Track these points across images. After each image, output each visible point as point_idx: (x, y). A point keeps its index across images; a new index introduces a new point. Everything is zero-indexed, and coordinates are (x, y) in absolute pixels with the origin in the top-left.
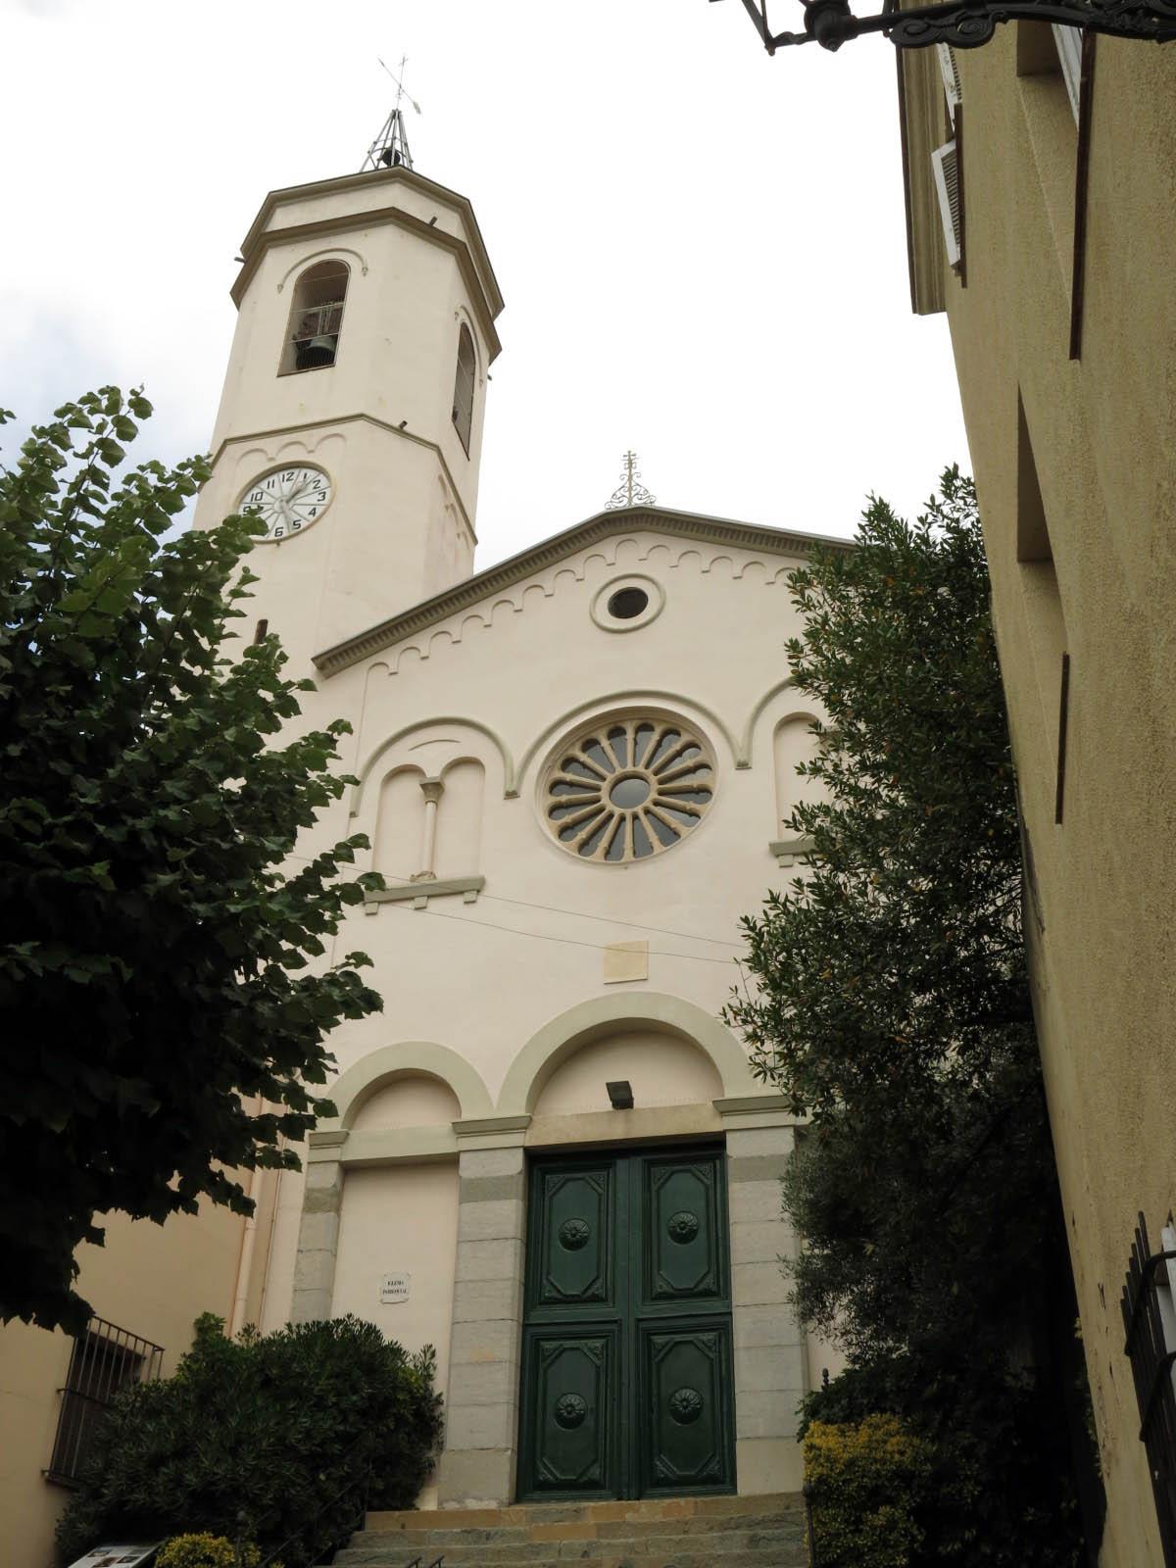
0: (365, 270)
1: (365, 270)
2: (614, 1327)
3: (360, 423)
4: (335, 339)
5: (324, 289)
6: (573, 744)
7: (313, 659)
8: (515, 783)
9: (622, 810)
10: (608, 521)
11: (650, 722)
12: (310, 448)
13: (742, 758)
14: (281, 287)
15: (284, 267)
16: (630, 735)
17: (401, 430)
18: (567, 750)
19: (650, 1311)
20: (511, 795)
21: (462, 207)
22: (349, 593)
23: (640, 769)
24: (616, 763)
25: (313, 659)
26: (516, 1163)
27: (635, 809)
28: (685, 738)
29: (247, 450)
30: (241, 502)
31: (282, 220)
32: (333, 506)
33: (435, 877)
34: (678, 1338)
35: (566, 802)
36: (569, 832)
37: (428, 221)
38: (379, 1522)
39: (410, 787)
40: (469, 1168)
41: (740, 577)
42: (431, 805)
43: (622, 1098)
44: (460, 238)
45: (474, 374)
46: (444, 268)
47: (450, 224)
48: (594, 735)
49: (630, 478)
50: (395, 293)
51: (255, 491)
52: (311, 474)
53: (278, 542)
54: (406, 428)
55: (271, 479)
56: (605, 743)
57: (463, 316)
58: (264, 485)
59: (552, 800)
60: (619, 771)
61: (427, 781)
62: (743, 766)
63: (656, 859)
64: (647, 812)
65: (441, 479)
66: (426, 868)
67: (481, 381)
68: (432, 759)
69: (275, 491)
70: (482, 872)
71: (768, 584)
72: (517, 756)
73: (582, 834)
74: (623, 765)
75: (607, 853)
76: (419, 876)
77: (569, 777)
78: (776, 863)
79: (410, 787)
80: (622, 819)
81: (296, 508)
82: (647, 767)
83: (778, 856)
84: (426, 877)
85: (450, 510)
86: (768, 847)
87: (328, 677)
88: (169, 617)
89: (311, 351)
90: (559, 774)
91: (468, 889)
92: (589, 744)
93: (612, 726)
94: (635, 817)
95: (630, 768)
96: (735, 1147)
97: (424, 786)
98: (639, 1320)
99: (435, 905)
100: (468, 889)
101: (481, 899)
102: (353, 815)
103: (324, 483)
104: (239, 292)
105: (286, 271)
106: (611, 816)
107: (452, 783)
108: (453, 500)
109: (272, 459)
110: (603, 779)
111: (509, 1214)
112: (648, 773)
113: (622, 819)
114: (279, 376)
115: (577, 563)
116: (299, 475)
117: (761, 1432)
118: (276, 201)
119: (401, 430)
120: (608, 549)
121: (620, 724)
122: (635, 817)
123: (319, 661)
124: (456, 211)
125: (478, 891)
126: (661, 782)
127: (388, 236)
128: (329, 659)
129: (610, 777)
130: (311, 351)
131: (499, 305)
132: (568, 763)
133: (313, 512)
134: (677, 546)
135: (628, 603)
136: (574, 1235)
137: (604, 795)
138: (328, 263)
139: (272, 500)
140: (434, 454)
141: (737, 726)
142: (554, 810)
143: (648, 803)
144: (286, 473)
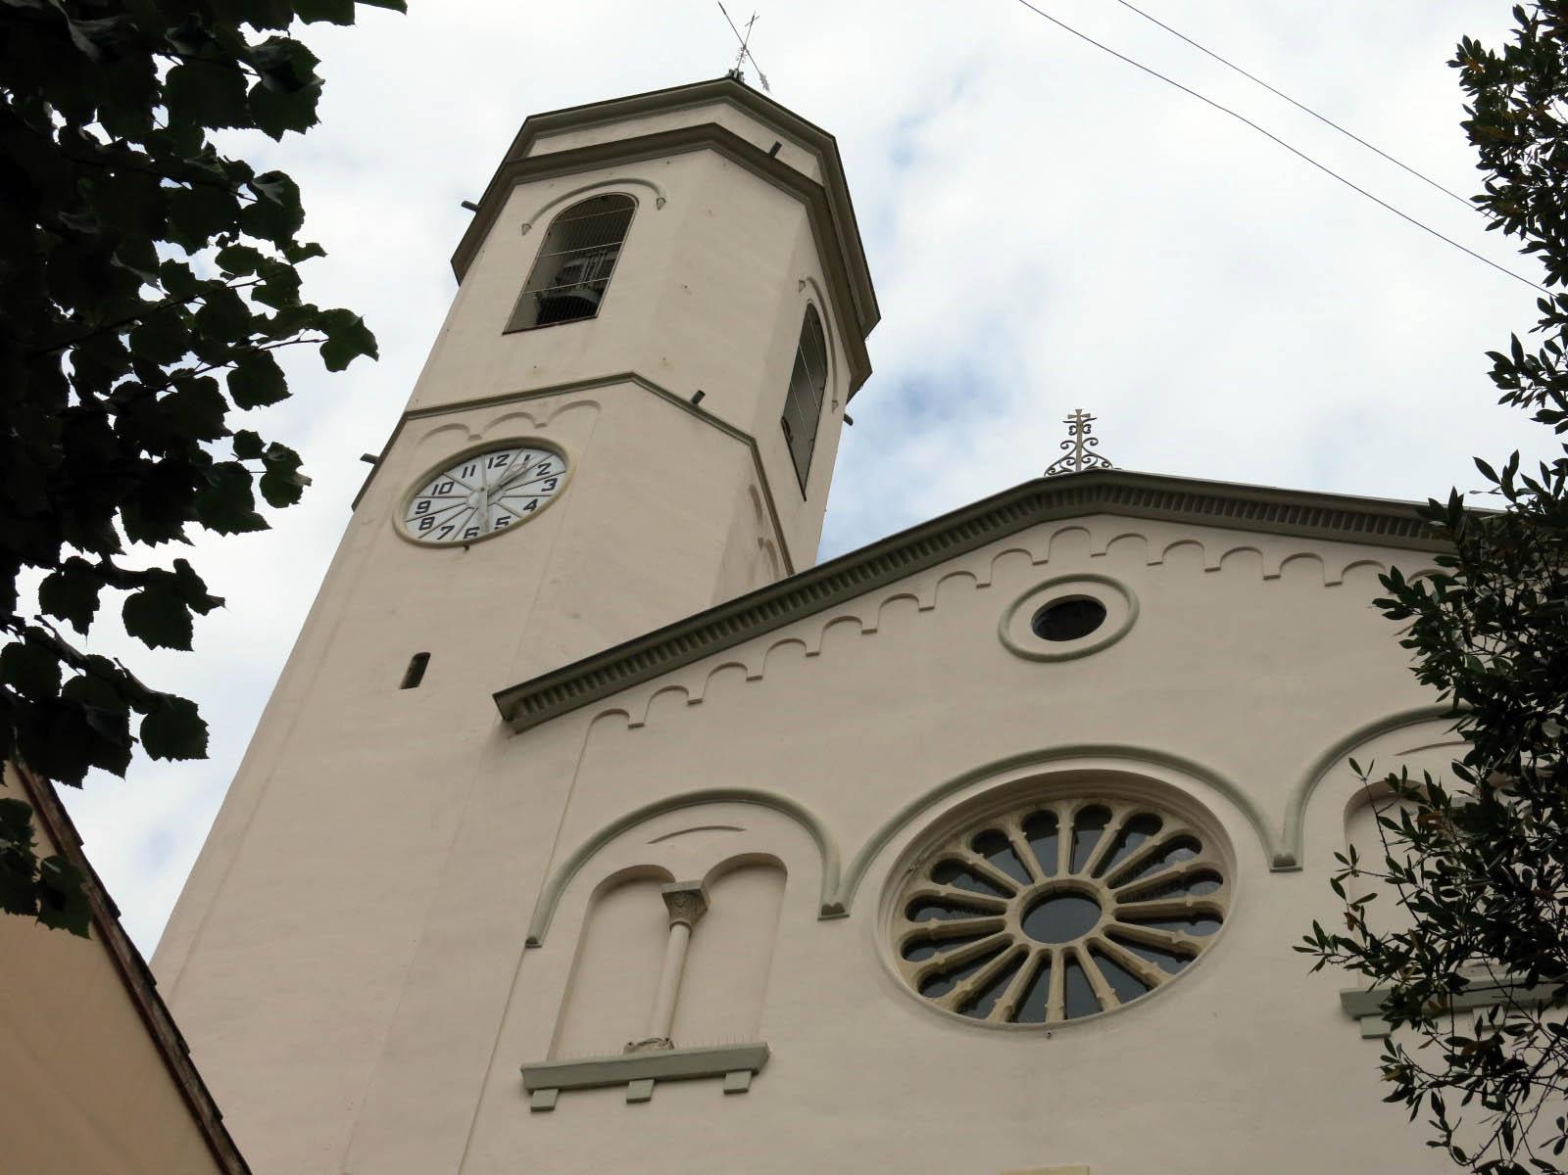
0: (661, 202)
1: (661, 202)
3: (629, 387)
4: (600, 291)
5: (590, 241)
6: (956, 837)
7: (497, 696)
8: (842, 890)
9: (1042, 946)
10: (1038, 497)
11: (1105, 802)
12: (539, 422)
13: (1284, 851)
14: (526, 228)
15: (536, 207)
16: (1065, 824)
17: (692, 405)
18: (942, 847)
20: (833, 912)
21: (823, 145)
22: (576, 616)
23: (1084, 876)
24: (1035, 867)
25: (497, 696)
27: (1071, 944)
28: (1170, 827)
29: (437, 426)
30: (416, 495)
31: (541, 148)
32: (568, 492)
33: (672, 1046)
35: (937, 932)
36: (941, 985)
37: (767, 149)
39: (645, 907)
41: (1277, 577)
42: (679, 931)
44: (816, 180)
45: (823, 389)
46: (786, 223)
47: (802, 162)
48: (996, 823)
49: (1079, 446)
50: (696, 230)
51: (441, 481)
52: (537, 457)
53: (466, 545)
54: (702, 404)
55: (469, 465)
56: (1017, 836)
57: (809, 293)
58: (457, 473)
59: (909, 927)
60: (1042, 880)
61: (675, 888)
62: (1285, 865)
63: (1109, 1020)
64: (1095, 950)
65: (753, 491)
66: (658, 1033)
67: (835, 401)
68: (688, 857)
69: (476, 481)
70: (766, 1036)
71: (1328, 585)
72: (848, 851)
73: (965, 985)
74: (1050, 868)
75: (1014, 1015)
76: (642, 1044)
77: (946, 890)
78: (1355, 1031)
79: (645, 907)
80: (1045, 962)
81: (504, 501)
82: (1097, 872)
83: (1358, 1018)
84: (656, 1046)
85: (765, 549)
86: (1337, 1001)
87: (519, 731)
88: (105, 139)
89: (563, 297)
90: (925, 885)
91: (735, 1068)
92: (991, 842)
93: (1031, 809)
94: (1071, 960)
95: (1063, 875)
97: (669, 898)
99: (667, 1097)
100: (735, 1068)
101: (758, 1086)
102: (532, 943)
103: (556, 467)
104: (463, 260)
105: (539, 208)
106: (1022, 956)
107: (721, 899)
108: (772, 536)
109: (477, 437)
110: (1010, 893)
112: (1100, 883)
113: (1045, 962)
114: (504, 333)
115: (980, 562)
116: (516, 460)
118: (536, 127)
119: (692, 405)
120: (1038, 541)
121: (1048, 807)
122: (1071, 960)
123: (504, 701)
124: (814, 153)
125: (755, 1073)
126: (1120, 899)
127: (700, 168)
128: (526, 701)
129: (1024, 891)
130: (563, 297)
131: (873, 316)
132: (948, 869)
133: (532, 506)
134: (1158, 536)
135: (1069, 618)
137: (1014, 907)
138: (605, 198)
139: (467, 492)
140: (744, 450)
141: (1273, 799)
142: (911, 947)
143: (1097, 933)
144: (495, 456)
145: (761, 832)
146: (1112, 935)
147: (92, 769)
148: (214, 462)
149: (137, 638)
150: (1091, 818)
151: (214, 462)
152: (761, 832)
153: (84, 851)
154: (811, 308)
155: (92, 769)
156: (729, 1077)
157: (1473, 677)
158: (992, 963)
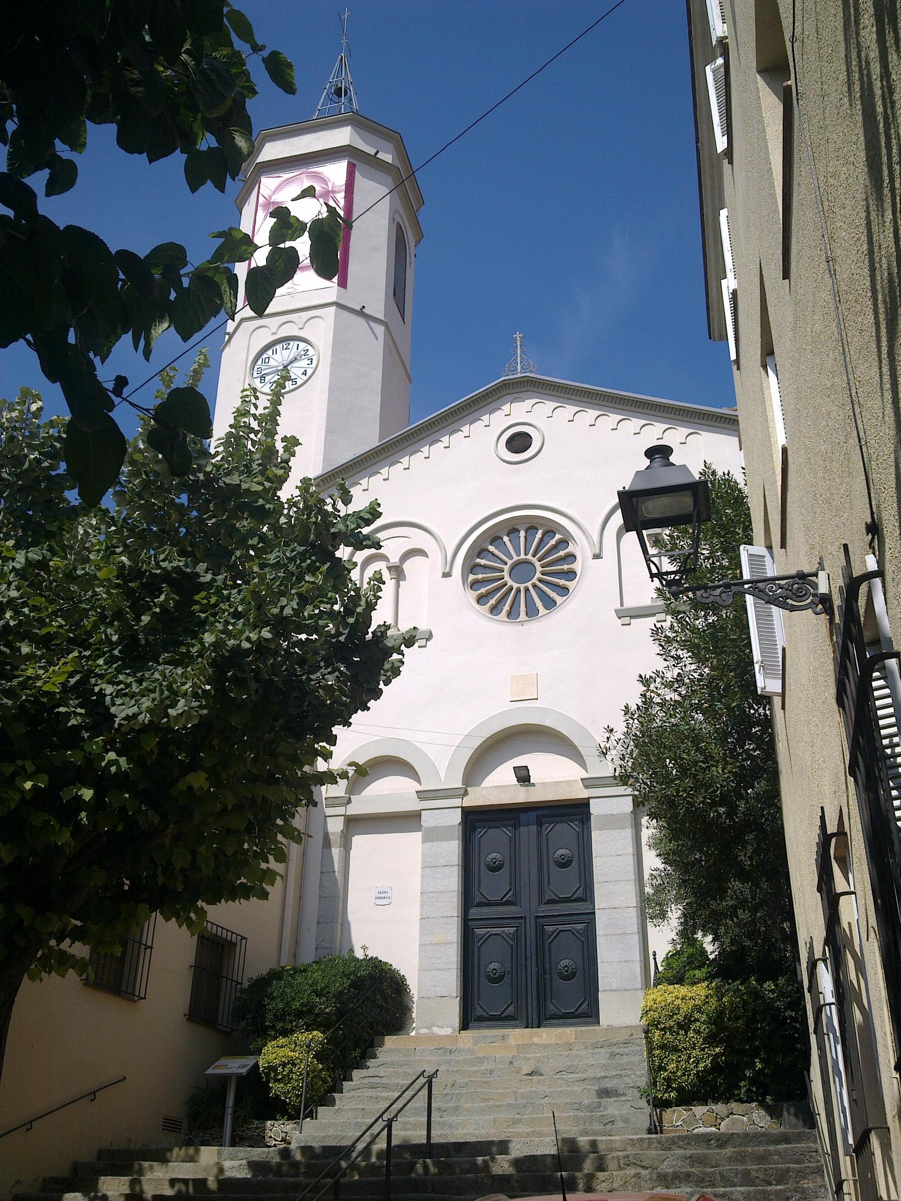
2: (523, 921)
9: (530, 583)
16: (522, 534)
19: (545, 910)
20: (447, 575)
26: (456, 817)
34: (561, 927)
38: (390, 1041)
40: (427, 820)
43: (523, 776)
60: (515, 558)
75: (509, 615)
80: (519, 590)
94: (527, 589)
96: (595, 808)
98: (537, 917)
111: (452, 849)
117: (614, 987)
136: (495, 863)
145: (417, 539)
146: (540, 581)
147: (59, 383)
148: (61, 228)
149: (40, 213)
150: (513, 531)
151: (61, 228)
152: (417, 539)
153: (20, 998)
154: (398, 224)
155: (59, 383)
156: (782, 711)
157: (96, 582)
158: (499, 594)
